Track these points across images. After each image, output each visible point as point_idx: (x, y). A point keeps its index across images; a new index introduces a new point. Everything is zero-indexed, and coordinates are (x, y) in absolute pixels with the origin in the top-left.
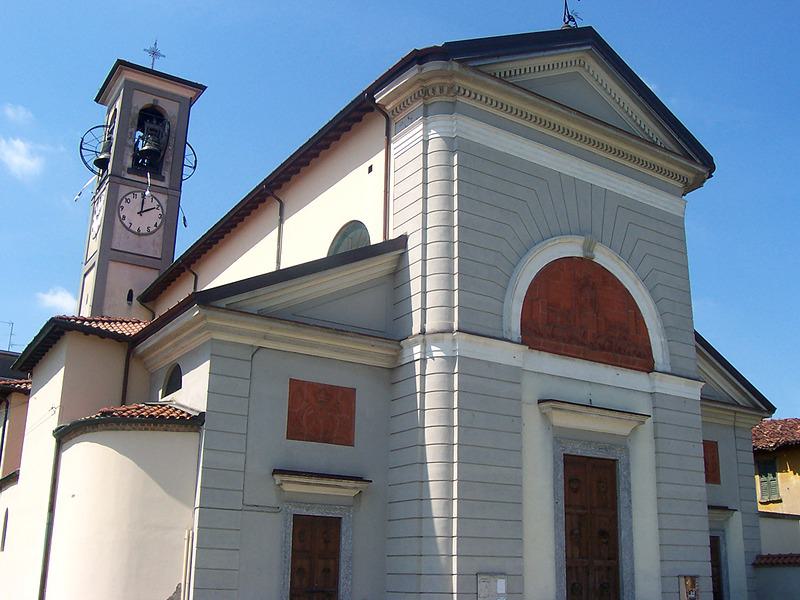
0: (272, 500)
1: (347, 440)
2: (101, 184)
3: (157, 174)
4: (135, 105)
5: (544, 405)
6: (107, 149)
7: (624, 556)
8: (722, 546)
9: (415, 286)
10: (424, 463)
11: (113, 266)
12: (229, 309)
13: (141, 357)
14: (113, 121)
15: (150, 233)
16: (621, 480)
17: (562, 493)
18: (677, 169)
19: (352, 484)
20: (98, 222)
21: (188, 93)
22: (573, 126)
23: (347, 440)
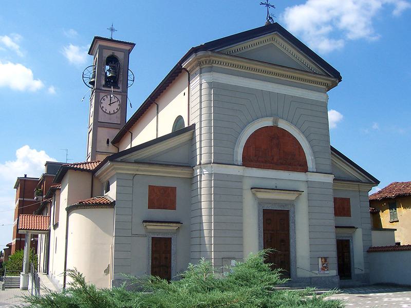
0: (143, 232)
1: (172, 206)
2: (93, 92)
3: (116, 86)
4: (104, 56)
5: (253, 190)
6: (94, 77)
7: (292, 250)
8: (351, 244)
9: (198, 145)
10: (201, 216)
11: (99, 129)
12: (122, 161)
13: (97, 178)
14: (96, 64)
15: (115, 113)
17: (262, 225)
18: (319, 80)
19: (175, 225)
20: (92, 110)
21: (128, 48)
22: (258, 67)
23: (172, 206)
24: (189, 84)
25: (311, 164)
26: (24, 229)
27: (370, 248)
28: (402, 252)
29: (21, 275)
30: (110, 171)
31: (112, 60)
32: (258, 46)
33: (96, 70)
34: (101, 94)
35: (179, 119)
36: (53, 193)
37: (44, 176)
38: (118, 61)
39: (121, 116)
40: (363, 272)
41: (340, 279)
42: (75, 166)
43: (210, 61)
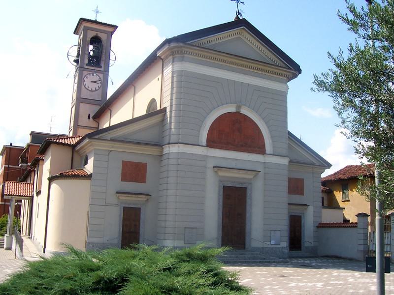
11: (82, 105)
12: (99, 139)
14: (80, 44)
15: (96, 90)
16: (248, 195)
19: (144, 196)
21: (111, 30)
22: (234, 60)
24: (163, 71)
25: (269, 148)
26: (9, 195)
27: (320, 224)
28: (345, 228)
29: (5, 236)
30: (89, 147)
31: (96, 41)
32: (226, 39)
33: (81, 50)
34: (84, 72)
35: (153, 101)
36: (37, 163)
37: (29, 146)
38: (101, 42)
39: (102, 94)
40: (312, 245)
41: (290, 250)
42: (58, 141)
43: (181, 52)
